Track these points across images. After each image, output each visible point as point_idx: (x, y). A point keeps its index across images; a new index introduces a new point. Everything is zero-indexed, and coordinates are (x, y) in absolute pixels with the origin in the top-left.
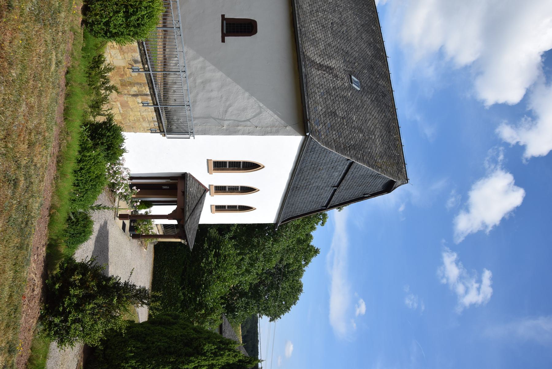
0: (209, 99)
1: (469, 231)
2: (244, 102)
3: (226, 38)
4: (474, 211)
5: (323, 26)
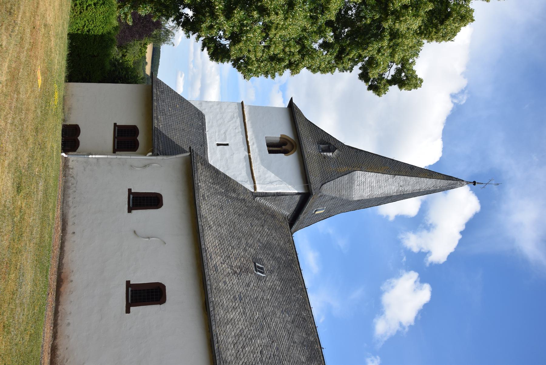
1: (389, 334)
3: (132, 309)
4: (389, 313)
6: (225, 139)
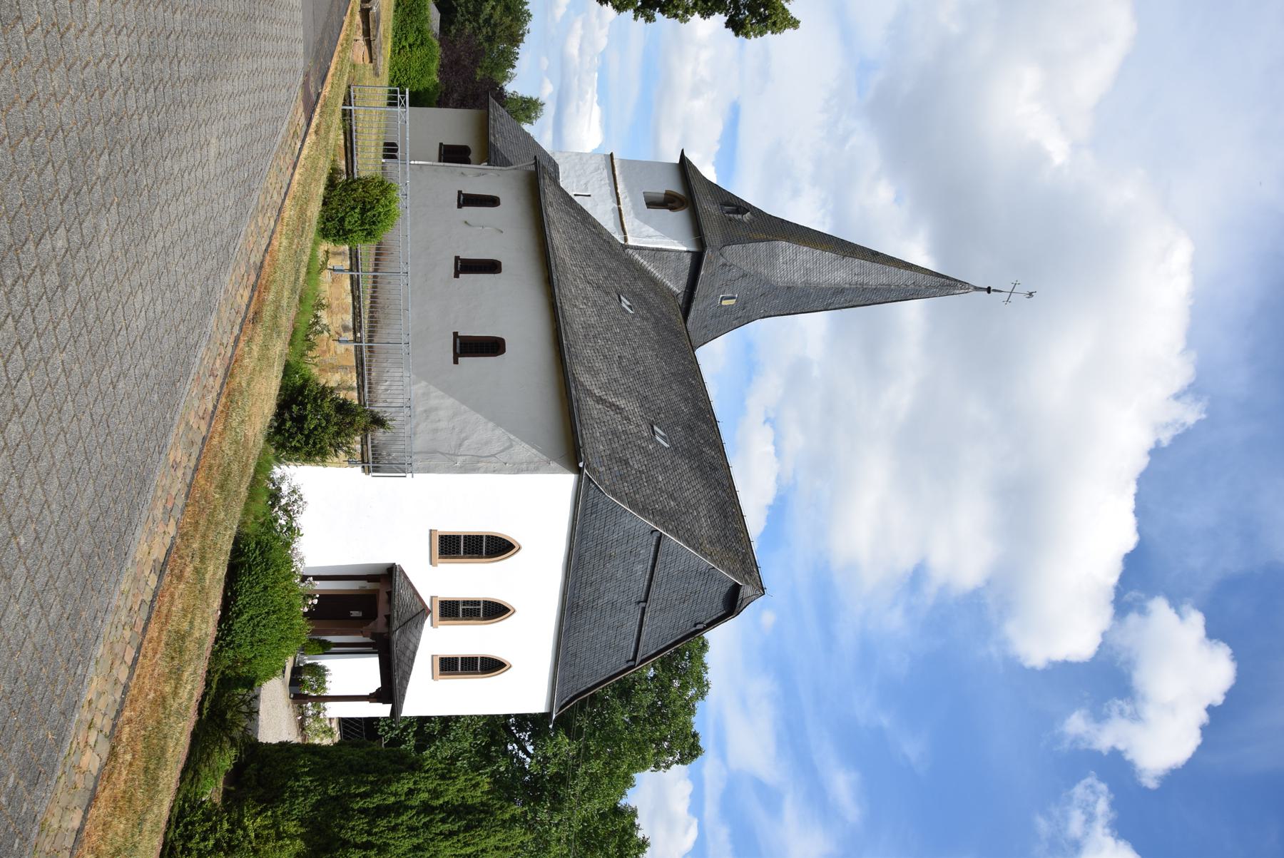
0: (436, 431)
2: (486, 433)
5: (605, 357)
6: (586, 189)
